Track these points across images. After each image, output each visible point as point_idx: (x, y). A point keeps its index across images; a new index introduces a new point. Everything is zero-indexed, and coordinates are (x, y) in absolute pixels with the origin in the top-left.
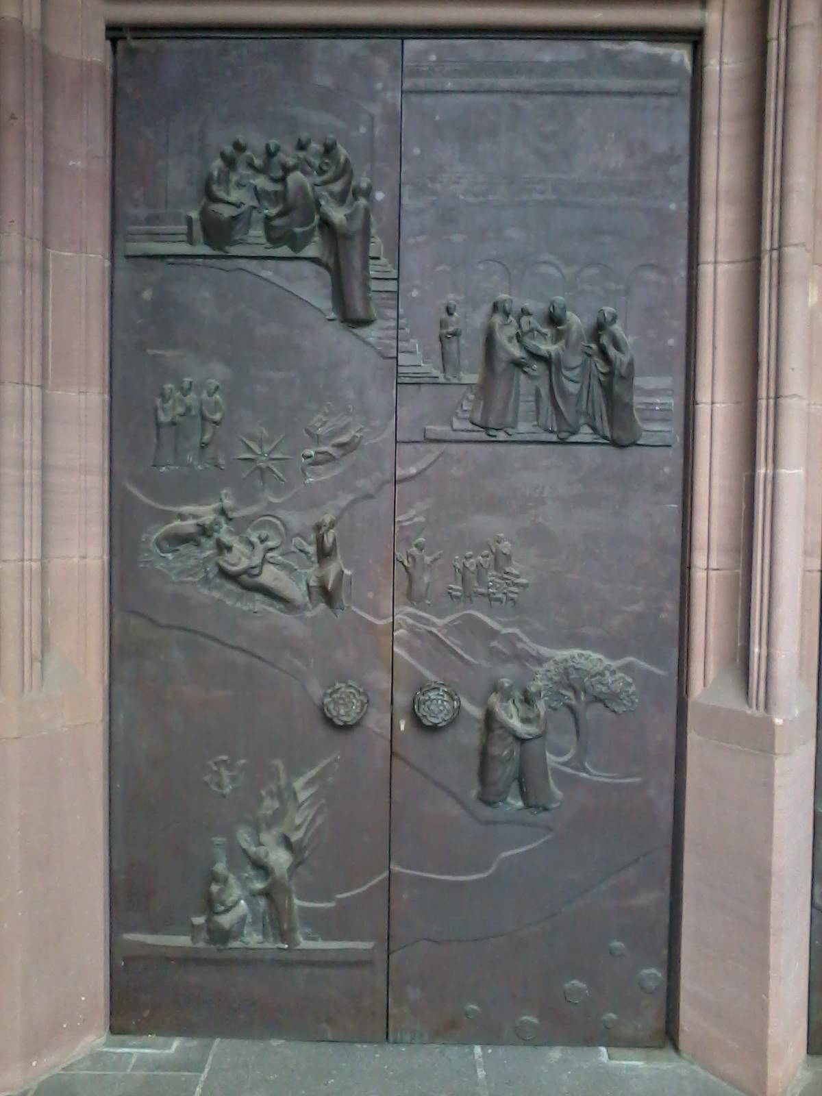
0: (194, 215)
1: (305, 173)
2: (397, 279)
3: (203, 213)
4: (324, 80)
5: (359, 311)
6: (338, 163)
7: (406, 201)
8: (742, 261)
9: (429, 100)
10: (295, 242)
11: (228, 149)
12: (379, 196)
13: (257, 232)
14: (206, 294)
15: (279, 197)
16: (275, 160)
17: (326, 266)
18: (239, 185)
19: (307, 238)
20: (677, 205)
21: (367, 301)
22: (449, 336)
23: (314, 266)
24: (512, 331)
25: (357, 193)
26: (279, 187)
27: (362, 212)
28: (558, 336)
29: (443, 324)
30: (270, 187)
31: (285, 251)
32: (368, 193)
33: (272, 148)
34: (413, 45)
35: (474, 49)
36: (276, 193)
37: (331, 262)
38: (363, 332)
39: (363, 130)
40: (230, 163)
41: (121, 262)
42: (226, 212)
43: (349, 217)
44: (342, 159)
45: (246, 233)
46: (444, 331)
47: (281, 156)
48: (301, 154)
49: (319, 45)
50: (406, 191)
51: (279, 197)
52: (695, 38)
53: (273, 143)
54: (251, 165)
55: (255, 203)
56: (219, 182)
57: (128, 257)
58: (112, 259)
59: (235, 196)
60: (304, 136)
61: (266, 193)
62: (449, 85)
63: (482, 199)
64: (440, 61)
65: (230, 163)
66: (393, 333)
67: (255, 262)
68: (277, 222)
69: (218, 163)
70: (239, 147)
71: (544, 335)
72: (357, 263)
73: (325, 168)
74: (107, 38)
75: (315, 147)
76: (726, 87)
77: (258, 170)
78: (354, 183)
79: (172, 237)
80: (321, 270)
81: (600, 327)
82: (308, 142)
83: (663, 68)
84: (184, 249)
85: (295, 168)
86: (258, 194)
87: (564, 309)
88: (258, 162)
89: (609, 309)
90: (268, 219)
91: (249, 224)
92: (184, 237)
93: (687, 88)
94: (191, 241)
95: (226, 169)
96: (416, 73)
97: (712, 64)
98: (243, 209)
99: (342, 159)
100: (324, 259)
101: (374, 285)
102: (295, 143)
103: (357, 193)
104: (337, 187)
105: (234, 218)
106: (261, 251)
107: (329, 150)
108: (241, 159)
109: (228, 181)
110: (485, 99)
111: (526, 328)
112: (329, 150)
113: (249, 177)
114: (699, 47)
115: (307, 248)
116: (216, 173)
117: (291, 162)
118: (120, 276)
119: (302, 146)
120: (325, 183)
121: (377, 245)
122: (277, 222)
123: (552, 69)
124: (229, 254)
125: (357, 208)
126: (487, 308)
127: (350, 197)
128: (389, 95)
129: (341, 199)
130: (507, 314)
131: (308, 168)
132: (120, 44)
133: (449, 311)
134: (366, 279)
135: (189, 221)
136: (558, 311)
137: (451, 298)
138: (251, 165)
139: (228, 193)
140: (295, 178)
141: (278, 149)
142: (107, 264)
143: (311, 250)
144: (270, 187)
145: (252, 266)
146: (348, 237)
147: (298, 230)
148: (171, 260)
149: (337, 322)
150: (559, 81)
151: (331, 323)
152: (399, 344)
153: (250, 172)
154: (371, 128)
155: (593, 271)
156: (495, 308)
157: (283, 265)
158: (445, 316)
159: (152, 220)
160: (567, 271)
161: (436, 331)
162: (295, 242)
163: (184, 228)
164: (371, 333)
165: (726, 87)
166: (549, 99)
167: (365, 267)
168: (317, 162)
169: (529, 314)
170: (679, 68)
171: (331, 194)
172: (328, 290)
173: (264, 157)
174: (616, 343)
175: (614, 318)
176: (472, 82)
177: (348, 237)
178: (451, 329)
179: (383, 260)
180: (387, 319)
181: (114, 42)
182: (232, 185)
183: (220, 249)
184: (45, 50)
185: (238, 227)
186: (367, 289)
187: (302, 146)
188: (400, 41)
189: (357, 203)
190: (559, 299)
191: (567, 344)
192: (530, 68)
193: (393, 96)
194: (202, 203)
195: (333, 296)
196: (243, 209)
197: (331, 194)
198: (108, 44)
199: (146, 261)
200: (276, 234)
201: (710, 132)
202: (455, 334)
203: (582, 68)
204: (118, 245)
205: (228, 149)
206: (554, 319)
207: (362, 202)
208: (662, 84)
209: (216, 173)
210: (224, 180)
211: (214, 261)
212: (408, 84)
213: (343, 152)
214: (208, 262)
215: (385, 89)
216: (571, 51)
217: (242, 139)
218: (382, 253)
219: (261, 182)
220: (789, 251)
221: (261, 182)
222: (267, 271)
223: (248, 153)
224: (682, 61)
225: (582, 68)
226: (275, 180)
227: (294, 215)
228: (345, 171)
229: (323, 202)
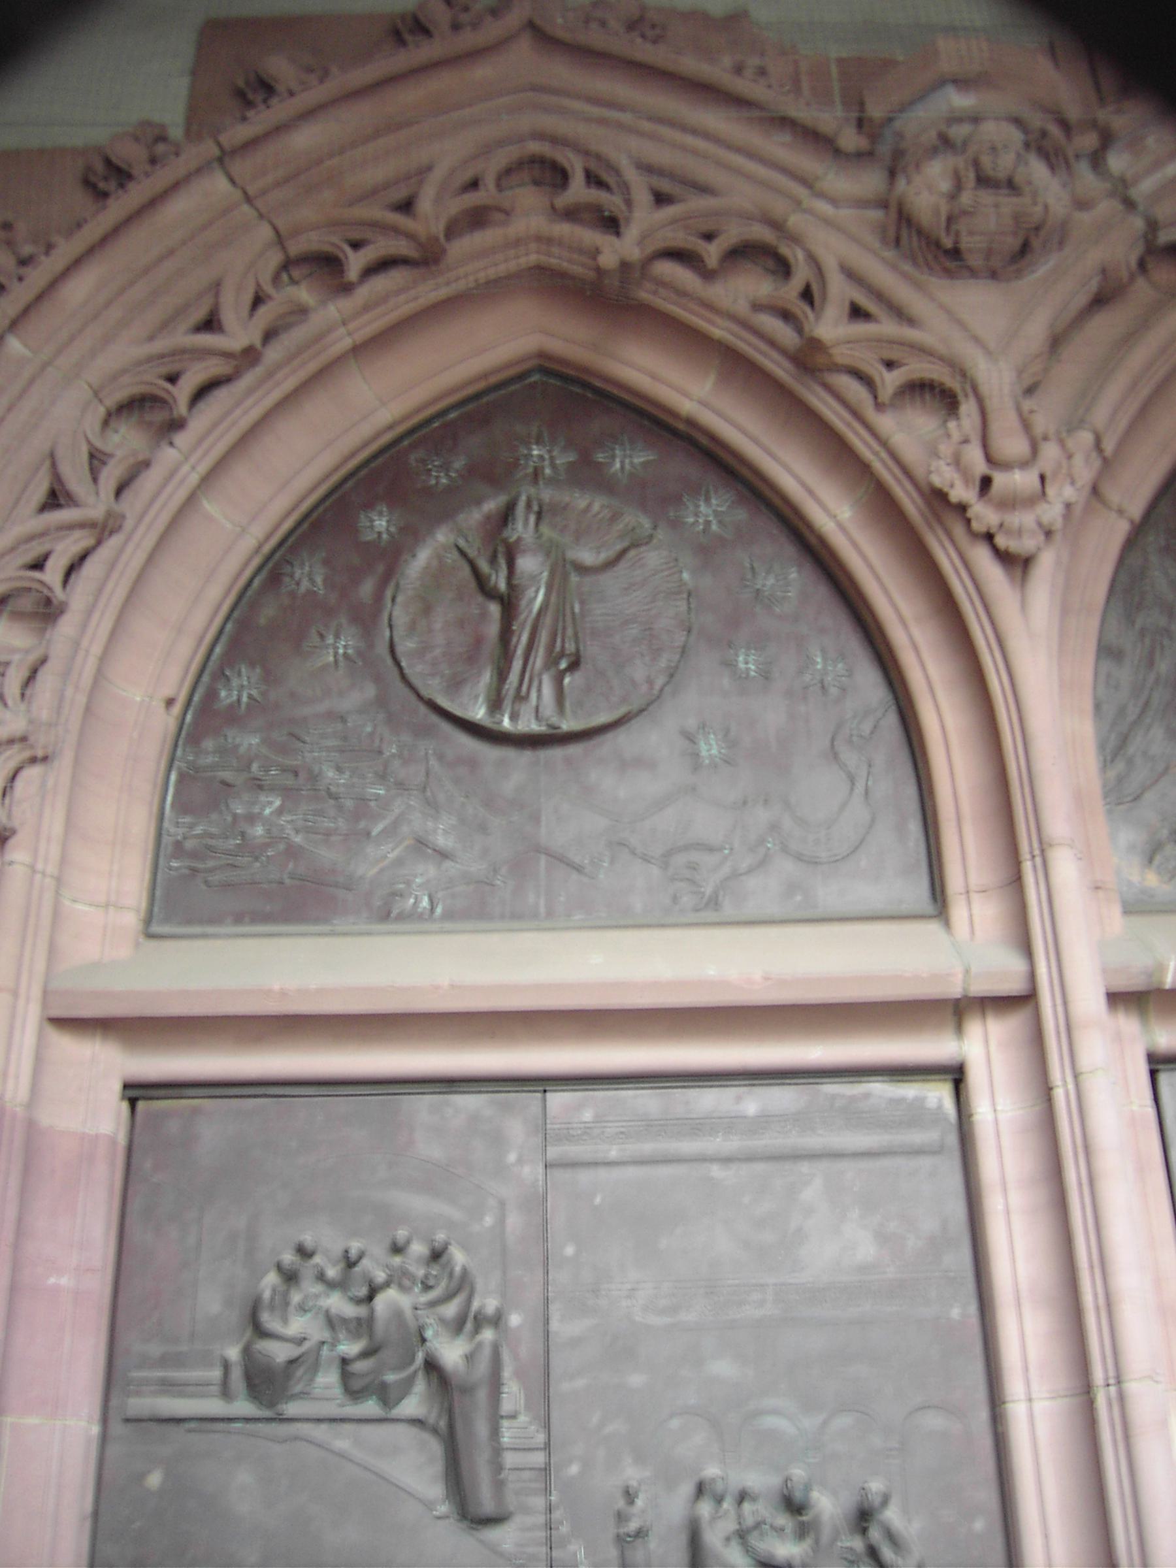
0: (233, 1353)
1: (402, 1288)
2: (547, 1446)
3: (247, 1351)
4: (430, 1149)
5: (487, 1504)
6: (451, 1275)
7: (554, 1325)
8: (1072, 1395)
9: (584, 1177)
10: (386, 1395)
11: (288, 1258)
12: (514, 1320)
13: (328, 1379)
14: (244, 1477)
15: (364, 1326)
16: (357, 1269)
17: (435, 1431)
18: (302, 1309)
19: (406, 1387)
20: (963, 1311)
21: (499, 1485)
22: (629, 1539)
23: (414, 1431)
24: (730, 1525)
25: (480, 1321)
26: (362, 1311)
27: (487, 1352)
28: (802, 1532)
29: (621, 1517)
30: (350, 1310)
31: (371, 1407)
32: (497, 1320)
33: (353, 1253)
34: (558, 1100)
35: (645, 1100)
36: (359, 1320)
37: (443, 1424)
38: (493, 1534)
39: (489, 1220)
40: (290, 1277)
41: (117, 1428)
42: (279, 1352)
43: (469, 1358)
44: (458, 1269)
45: (312, 1380)
46: (622, 1531)
47: (366, 1263)
48: (397, 1260)
49: (422, 1105)
50: (555, 1311)
51: (364, 1326)
52: (956, 1075)
53: (355, 1246)
54: (321, 1277)
55: (326, 1335)
56: (272, 1308)
57: (127, 1420)
58: (105, 1420)
59: (297, 1325)
60: (402, 1234)
61: (344, 1321)
62: (614, 1153)
63: (667, 1320)
64: (599, 1119)
65: (290, 1277)
66: (542, 1534)
67: (324, 1427)
68: (360, 1366)
69: (272, 1279)
70: (304, 1252)
71: (780, 1530)
72: (482, 1429)
73: (431, 1282)
74: (123, 1098)
75: (418, 1249)
76: (1006, 1141)
77: (331, 1285)
78: (476, 1305)
79: (198, 1389)
80: (427, 1436)
81: (863, 1517)
82: (408, 1242)
83: (916, 1115)
84: (214, 1406)
85: (387, 1284)
86: (332, 1322)
87: (808, 1488)
88: (332, 1273)
89: (876, 1486)
90: (345, 1361)
91: (315, 1368)
92: (215, 1389)
93: (952, 1139)
94: (226, 1392)
95: (282, 1288)
96: (566, 1137)
97: (982, 1110)
98: (306, 1346)
99: (458, 1269)
100: (432, 1420)
101: (510, 1459)
102: (387, 1243)
103: (480, 1321)
104: (451, 1310)
105: (292, 1362)
106: (331, 1410)
107: (437, 1255)
108: (307, 1271)
109: (287, 1304)
110: (664, 1171)
111: (750, 1521)
112: (437, 1255)
113: (317, 1296)
114: (962, 1086)
115: (405, 1402)
116: (267, 1295)
117: (380, 1276)
118: (113, 1450)
119: (397, 1249)
120: (433, 1304)
121: (513, 1395)
122: (360, 1366)
123: (763, 1122)
124: (284, 1417)
125: (480, 1345)
126: (687, 1489)
127: (469, 1326)
128: (527, 1170)
129: (458, 1326)
130: (719, 1500)
131: (407, 1283)
132: (141, 1105)
133: (629, 1496)
134: (497, 1451)
135: (226, 1366)
136: (798, 1495)
137: (632, 1474)
138: (321, 1277)
139: (285, 1321)
140: (382, 1302)
141: (361, 1256)
142: (95, 1430)
143: (412, 1406)
144: (350, 1310)
145: (320, 1432)
146: (467, 1390)
147: (391, 1377)
148: (193, 1425)
149: (452, 1520)
150: (769, 1141)
151: (440, 1523)
152: (554, 1554)
153: (318, 1288)
154: (501, 1221)
155: (844, 1421)
156: (701, 1490)
157: (367, 1430)
158: (621, 1503)
159: (164, 1361)
160: (810, 1423)
161: (612, 1531)
162: (386, 1395)
163: (216, 1374)
164: (505, 1537)
165: (1006, 1141)
166: (760, 1167)
167: (495, 1432)
168: (421, 1272)
169: (754, 1499)
170: (937, 1115)
171: (442, 1321)
172: (438, 1467)
173: (342, 1265)
174: (891, 1537)
175: (886, 1500)
176: (648, 1147)
177: (467, 1390)
178: (633, 1526)
179: (523, 1419)
180: (527, 1510)
181: (133, 1102)
182: (291, 1309)
183: (271, 1405)
184: (31, 1125)
185: (300, 1372)
186: (498, 1467)
187: (397, 1249)
188: (539, 1095)
189: (479, 1337)
190: (798, 1473)
191: (817, 1541)
192: (731, 1124)
193: (532, 1172)
194: (245, 1339)
195: (447, 1475)
196: (306, 1346)
197: (442, 1321)
198: (125, 1106)
199: (153, 1426)
200: (356, 1384)
201: (994, 1205)
202: (640, 1534)
203: (800, 1120)
204: (114, 1402)
205: (288, 1258)
206: (793, 1505)
207: (488, 1335)
208: (917, 1137)
209: (267, 1295)
210: (282, 1305)
211: (260, 1426)
212: (553, 1152)
213: (459, 1257)
214: (250, 1426)
215: (520, 1161)
216: (783, 1097)
217: (308, 1239)
218: (523, 1406)
219: (336, 1303)
220: (1133, 1387)
221: (336, 1303)
222: (342, 1440)
223: (317, 1259)
224: (940, 1107)
225: (800, 1120)
226: (358, 1301)
227: (384, 1355)
228: (463, 1284)
229: (429, 1334)
